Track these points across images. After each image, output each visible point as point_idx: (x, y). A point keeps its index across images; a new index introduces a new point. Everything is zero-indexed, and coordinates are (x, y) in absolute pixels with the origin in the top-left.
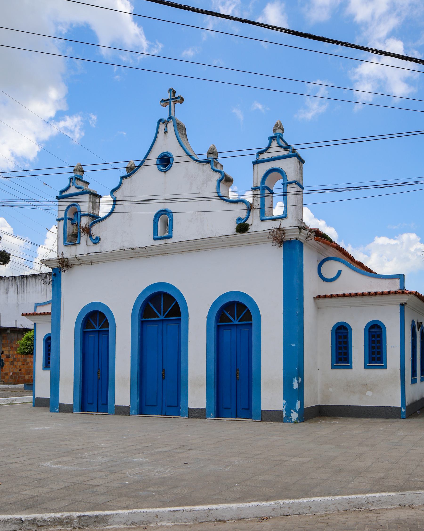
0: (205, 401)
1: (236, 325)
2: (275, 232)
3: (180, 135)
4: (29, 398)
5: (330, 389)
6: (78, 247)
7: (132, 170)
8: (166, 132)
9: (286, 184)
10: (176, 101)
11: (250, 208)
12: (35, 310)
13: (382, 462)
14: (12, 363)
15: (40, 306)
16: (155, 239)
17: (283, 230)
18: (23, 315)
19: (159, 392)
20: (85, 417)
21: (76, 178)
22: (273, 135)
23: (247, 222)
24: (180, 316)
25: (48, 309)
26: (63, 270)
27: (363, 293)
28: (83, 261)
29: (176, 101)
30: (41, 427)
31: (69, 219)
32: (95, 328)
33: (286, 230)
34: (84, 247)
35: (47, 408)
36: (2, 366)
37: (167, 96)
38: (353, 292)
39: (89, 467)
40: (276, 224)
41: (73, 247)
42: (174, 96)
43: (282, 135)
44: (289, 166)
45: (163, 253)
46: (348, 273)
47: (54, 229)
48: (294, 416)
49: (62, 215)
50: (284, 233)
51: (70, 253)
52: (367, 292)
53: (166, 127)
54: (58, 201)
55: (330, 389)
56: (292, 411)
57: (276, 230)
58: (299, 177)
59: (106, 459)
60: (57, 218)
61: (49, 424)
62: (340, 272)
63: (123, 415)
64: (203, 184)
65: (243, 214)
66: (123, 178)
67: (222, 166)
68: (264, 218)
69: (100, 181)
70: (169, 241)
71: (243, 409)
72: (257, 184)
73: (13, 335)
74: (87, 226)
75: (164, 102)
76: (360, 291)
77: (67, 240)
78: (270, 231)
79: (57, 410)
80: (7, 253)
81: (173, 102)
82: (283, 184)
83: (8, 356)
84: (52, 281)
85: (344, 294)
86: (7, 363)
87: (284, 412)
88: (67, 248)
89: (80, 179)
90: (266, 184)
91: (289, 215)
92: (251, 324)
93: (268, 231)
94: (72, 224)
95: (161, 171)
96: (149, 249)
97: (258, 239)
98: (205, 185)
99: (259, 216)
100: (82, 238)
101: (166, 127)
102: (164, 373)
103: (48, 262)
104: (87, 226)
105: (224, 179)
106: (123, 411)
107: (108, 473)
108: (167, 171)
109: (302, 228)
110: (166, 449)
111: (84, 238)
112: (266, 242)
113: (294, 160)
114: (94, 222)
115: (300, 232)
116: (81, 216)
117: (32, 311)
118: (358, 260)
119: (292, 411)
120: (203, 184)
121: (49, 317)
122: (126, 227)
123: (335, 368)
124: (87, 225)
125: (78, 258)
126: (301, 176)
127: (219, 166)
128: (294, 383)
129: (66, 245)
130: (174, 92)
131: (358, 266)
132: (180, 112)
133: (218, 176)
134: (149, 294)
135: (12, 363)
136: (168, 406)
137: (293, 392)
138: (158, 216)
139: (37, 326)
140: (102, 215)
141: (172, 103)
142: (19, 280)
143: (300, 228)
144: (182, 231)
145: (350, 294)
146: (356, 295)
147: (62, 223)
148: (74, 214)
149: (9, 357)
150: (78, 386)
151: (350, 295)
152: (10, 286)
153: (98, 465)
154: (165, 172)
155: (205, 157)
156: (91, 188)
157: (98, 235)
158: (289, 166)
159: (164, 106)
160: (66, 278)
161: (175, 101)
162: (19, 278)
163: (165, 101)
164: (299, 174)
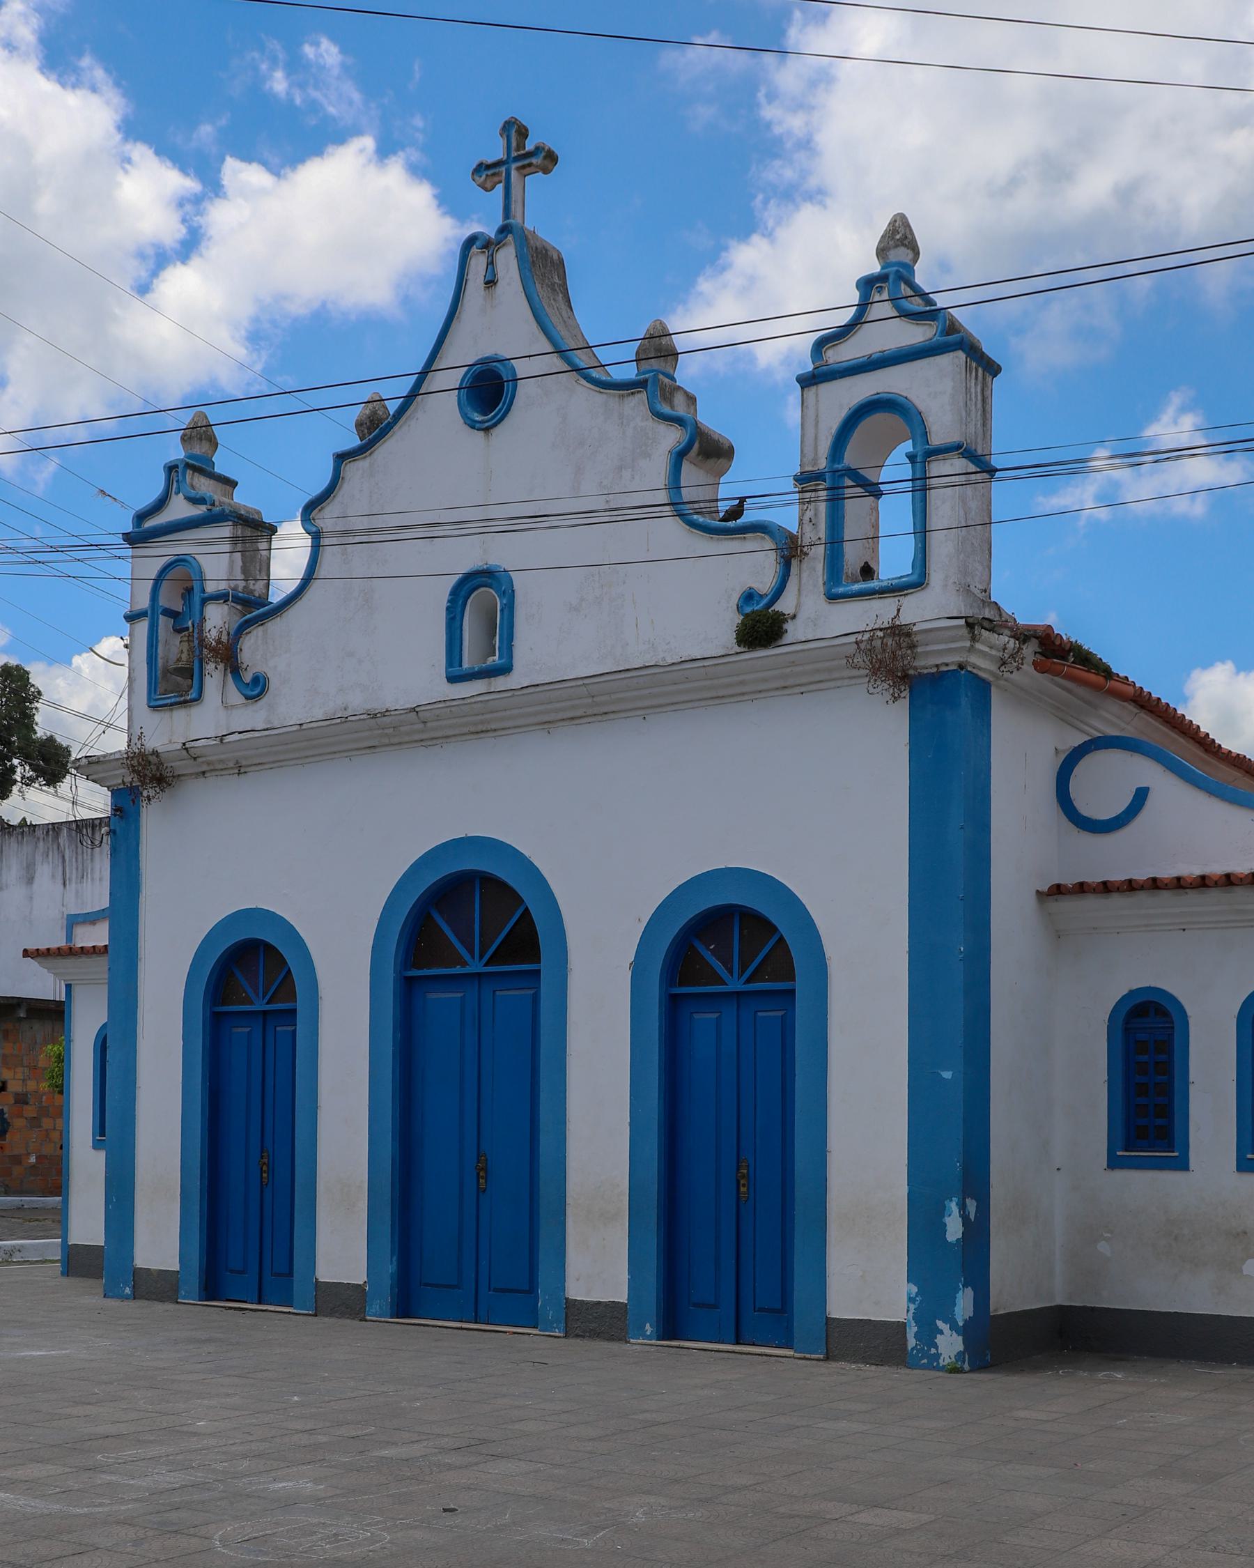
0: (625, 1276)
1: (738, 994)
2: (878, 643)
3: (541, 292)
4: (51, 1246)
5: (1103, 1247)
6: (195, 711)
7: (376, 428)
8: (491, 283)
9: (925, 456)
10: (530, 165)
11: (790, 551)
12: (70, 936)
13: (1215, 1549)
14: (35, 1122)
15: (84, 922)
16: (452, 679)
17: (909, 635)
18: (26, 953)
19: (464, 1242)
20: (216, 1315)
21: (188, 466)
22: (875, 268)
23: (779, 607)
24: (539, 961)
25: (97, 935)
26: (145, 793)
27: (1228, 876)
28: (209, 764)
29: (530, 165)
30: (39, 1348)
31: (168, 613)
32: (251, 1003)
33: (916, 633)
34: (214, 715)
35: (91, 1282)
36: (5, 1132)
37: (496, 150)
38: (1193, 870)
39: (101, 1505)
40: (879, 612)
41: (180, 714)
42: (521, 145)
43: (910, 269)
44: (933, 388)
45: (480, 728)
46: (1173, 800)
47: (112, 645)
48: (949, 1344)
49: (144, 602)
50: (912, 646)
51: (167, 733)
52: (1247, 872)
53: (491, 263)
54: (129, 552)
55: (1103, 1247)
56: (940, 1324)
57: (880, 634)
58: (974, 427)
59: (179, 1478)
60: (127, 609)
61: (87, 1339)
62: (1141, 796)
63: (343, 1315)
64: (620, 468)
65: (765, 582)
66: (342, 458)
67: (691, 400)
68: (841, 590)
69: (273, 472)
70: (500, 683)
71: (761, 1310)
72: (815, 461)
73: (37, 1026)
74: (224, 638)
75: (487, 172)
76: (1217, 868)
77: (160, 688)
78: (859, 637)
79: (128, 1291)
80: (60, 746)
81: (518, 169)
82: (912, 458)
83: (21, 1099)
84: (108, 834)
85: (1154, 880)
86: (18, 1123)
87: (912, 1330)
88: (157, 717)
89: (202, 467)
90: (851, 458)
91: (936, 577)
92: (792, 993)
93: (852, 639)
94: (178, 631)
95: (473, 427)
96: (428, 714)
97: (818, 671)
98: (627, 474)
99: (821, 582)
100: (207, 680)
101: (491, 263)
102: (485, 1169)
103: (95, 767)
104: (224, 638)
105: (696, 446)
106: (341, 1302)
107: (150, 1533)
108: (495, 425)
109: (983, 622)
110: (416, 1450)
111: (214, 678)
112: (846, 682)
113: (954, 361)
114: (247, 622)
115: (974, 639)
116: (204, 601)
117: (59, 941)
118: (1235, 750)
119: (940, 1324)
120: (620, 468)
121: (100, 966)
122: (359, 642)
123: (1122, 1167)
124: (225, 633)
125: (191, 751)
126: (984, 425)
127: (679, 399)
128: (947, 1220)
129: (155, 707)
130: (523, 133)
131: (1237, 774)
132: (545, 207)
133: (671, 437)
134: (431, 878)
135: (35, 1122)
136: (496, 1290)
137: (950, 1253)
138: (463, 593)
139: (77, 992)
140: (276, 597)
141: (514, 174)
142: (69, 836)
143: (970, 626)
144: (550, 645)
145: (1178, 879)
146: (1203, 882)
147: (143, 626)
148: (183, 596)
149: (27, 1103)
150: (196, 1208)
151: (1179, 884)
152: (39, 858)
153: (135, 1500)
154: (487, 430)
155: (629, 372)
156: (242, 498)
157: (259, 668)
158: (933, 388)
159: (488, 185)
160: (156, 823)
161: (523, 167)
162: (70, 829)
163: (489, 167)
164: (976, 415)
